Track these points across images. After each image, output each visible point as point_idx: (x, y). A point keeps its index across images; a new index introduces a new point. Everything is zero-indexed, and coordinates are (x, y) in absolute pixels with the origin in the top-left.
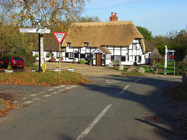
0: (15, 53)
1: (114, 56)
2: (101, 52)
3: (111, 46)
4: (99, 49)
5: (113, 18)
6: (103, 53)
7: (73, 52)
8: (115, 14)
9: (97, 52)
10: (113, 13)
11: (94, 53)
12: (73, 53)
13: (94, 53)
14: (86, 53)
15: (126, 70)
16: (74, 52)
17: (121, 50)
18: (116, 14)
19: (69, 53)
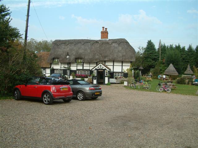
0: (110, 137)
1: (113, 72)
2: (103, 68)
3: (109, 61)
4: (102, 65)
5: (105, 33)
6: (107, 69)
7: (60, 68)
8: (105, 29)
9: (98, 68)
10: (107, 29)
11: (94, 69)
12: (60, 69)
13: (94, 69)
14: (78, 70)
15: (95, 88)
16: (62, 68)
17: (122, 66)
18: (107, 29)
19: (117, 72)
